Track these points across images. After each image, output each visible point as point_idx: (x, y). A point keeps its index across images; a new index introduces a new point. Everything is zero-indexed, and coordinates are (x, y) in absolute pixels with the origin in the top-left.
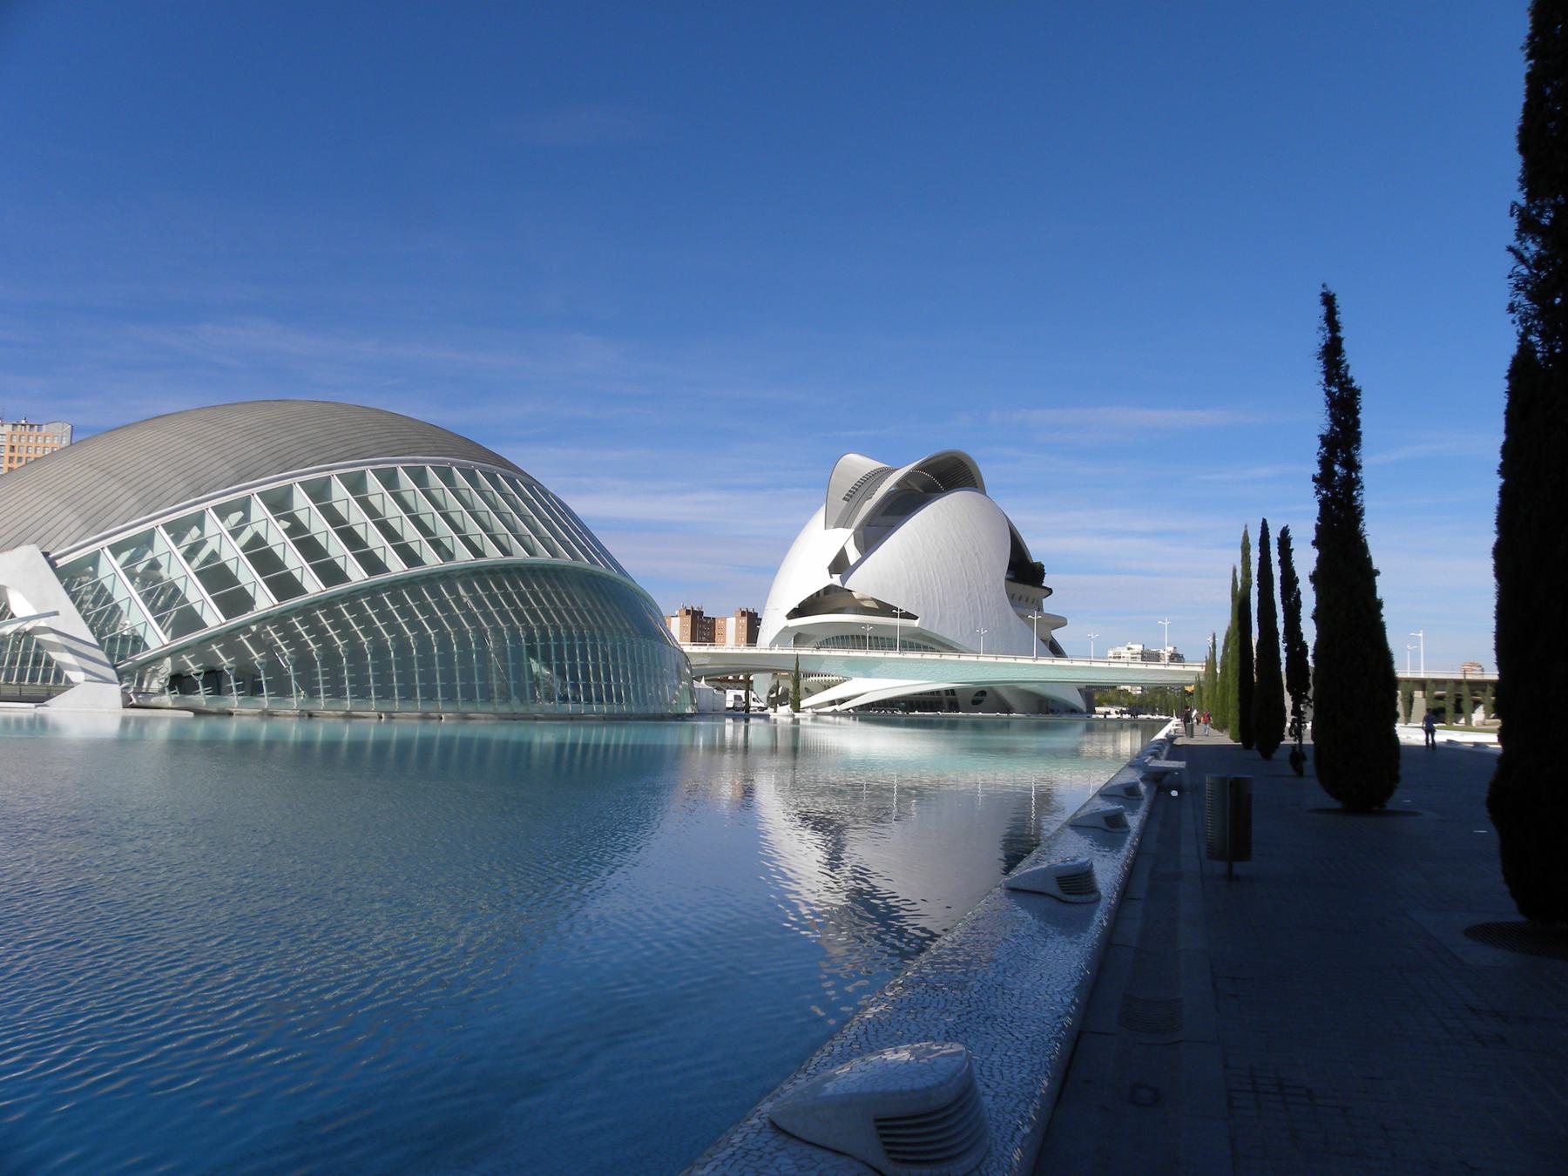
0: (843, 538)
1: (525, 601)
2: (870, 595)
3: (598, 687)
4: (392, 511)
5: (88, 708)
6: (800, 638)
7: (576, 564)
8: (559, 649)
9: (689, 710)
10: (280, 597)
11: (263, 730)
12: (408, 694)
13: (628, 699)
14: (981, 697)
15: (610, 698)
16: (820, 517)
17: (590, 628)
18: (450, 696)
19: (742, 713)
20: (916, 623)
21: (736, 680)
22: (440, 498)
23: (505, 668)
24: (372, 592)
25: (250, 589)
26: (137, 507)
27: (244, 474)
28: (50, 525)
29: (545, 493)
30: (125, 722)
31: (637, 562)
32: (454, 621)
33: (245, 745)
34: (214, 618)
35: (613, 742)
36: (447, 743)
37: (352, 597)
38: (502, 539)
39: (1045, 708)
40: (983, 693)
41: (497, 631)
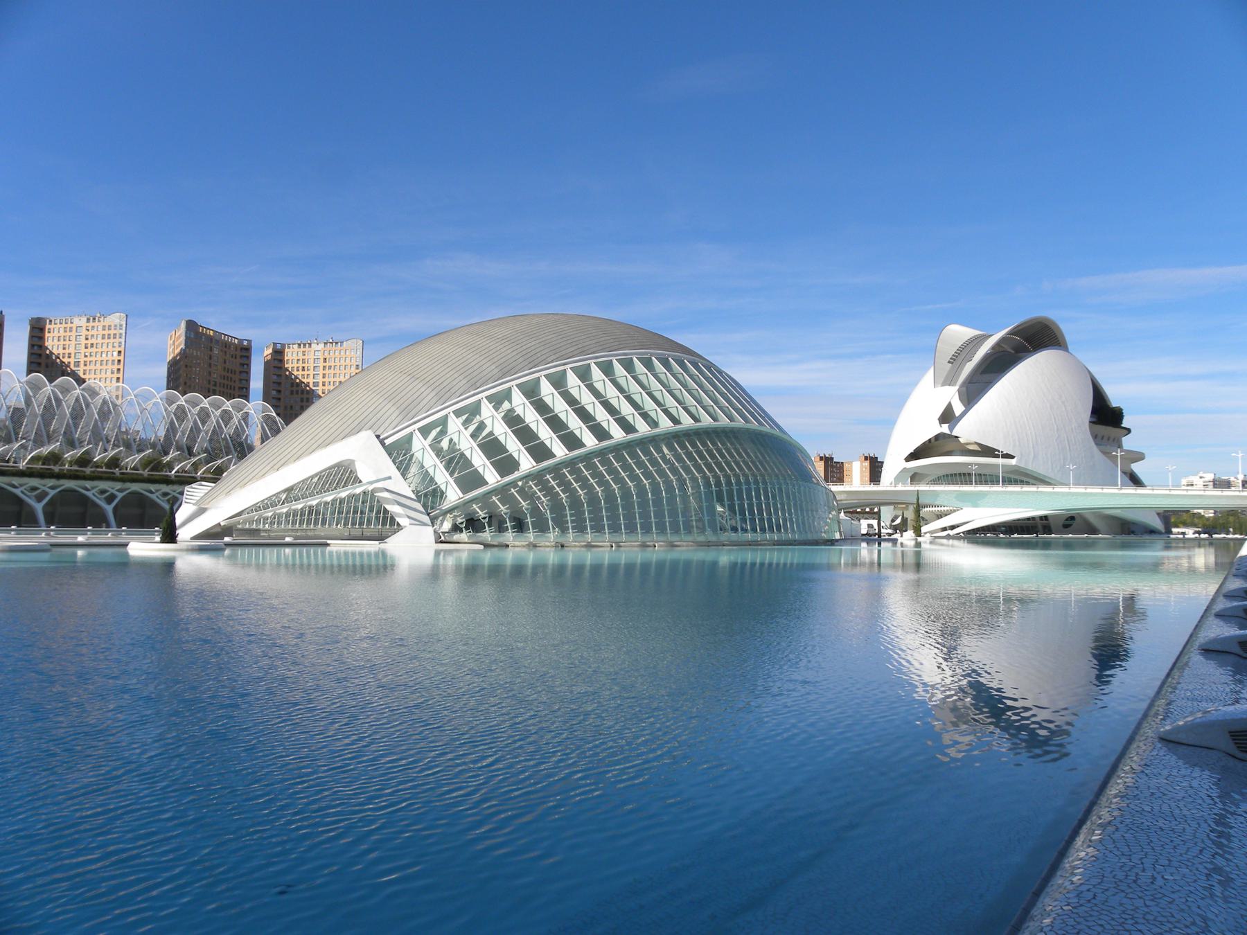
0: (950, 395)
1: (713, 456)
2: (973, 440)
3: (770, 520)
4: (611, 393)
5: (413, 545)
6: (915, 477)
7: (748, 426)
8: (740, 492)
9: (837, 536)
10: (538, 460)
11: (530, 558)
12: (631, 529)
13: (786, 529)
14: (1070, 522)
15: (779, 529)
16: (930, 375)
17: (762, 476)
18: (662, 529)
19: (874, 538)
20: (1013, 462)
21: (864, 512)
22: (645, 382)
23: (701, 508)
24: (601, 453)
25: (515, 455)
26: (434, 400)
27: (506, 372)
28: (378, 416)
29: (721, 372)
30: (437, 553)
31: (808, 428)
32: (661, 473)
33: (518, 570)
34: (492, 477)
35: (775, 561)
36: (661, 565)
37: (587, 458)
38: (693, 410)
39: (1127, 529)
40: (1072, 518)
41: (694, 479)
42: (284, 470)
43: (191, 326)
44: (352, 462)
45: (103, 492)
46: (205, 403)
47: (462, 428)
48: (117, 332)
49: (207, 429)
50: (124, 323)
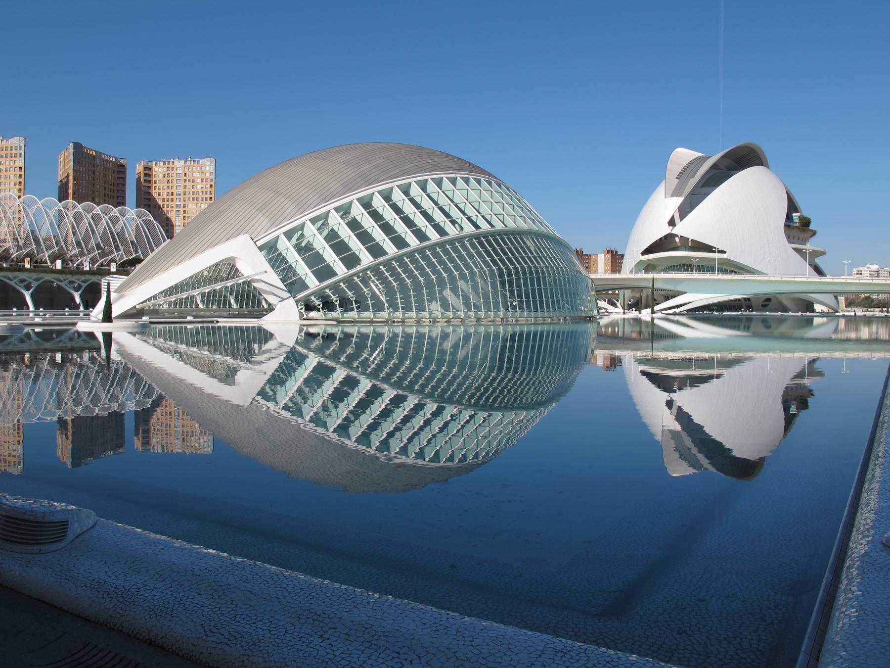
6: (649, 267)
10: (375, 257)
20: (724, 256)
26: (295, 211)
34: (341, 270)
40: (769, 300)
42: (182, 266)
43: (78, 147)
44: (233, 259)
45: (22, 281)
46: (98, 209)
47: (316, 232)
48: (19, 152)
49: (99, 230)
50: (23, 145)
